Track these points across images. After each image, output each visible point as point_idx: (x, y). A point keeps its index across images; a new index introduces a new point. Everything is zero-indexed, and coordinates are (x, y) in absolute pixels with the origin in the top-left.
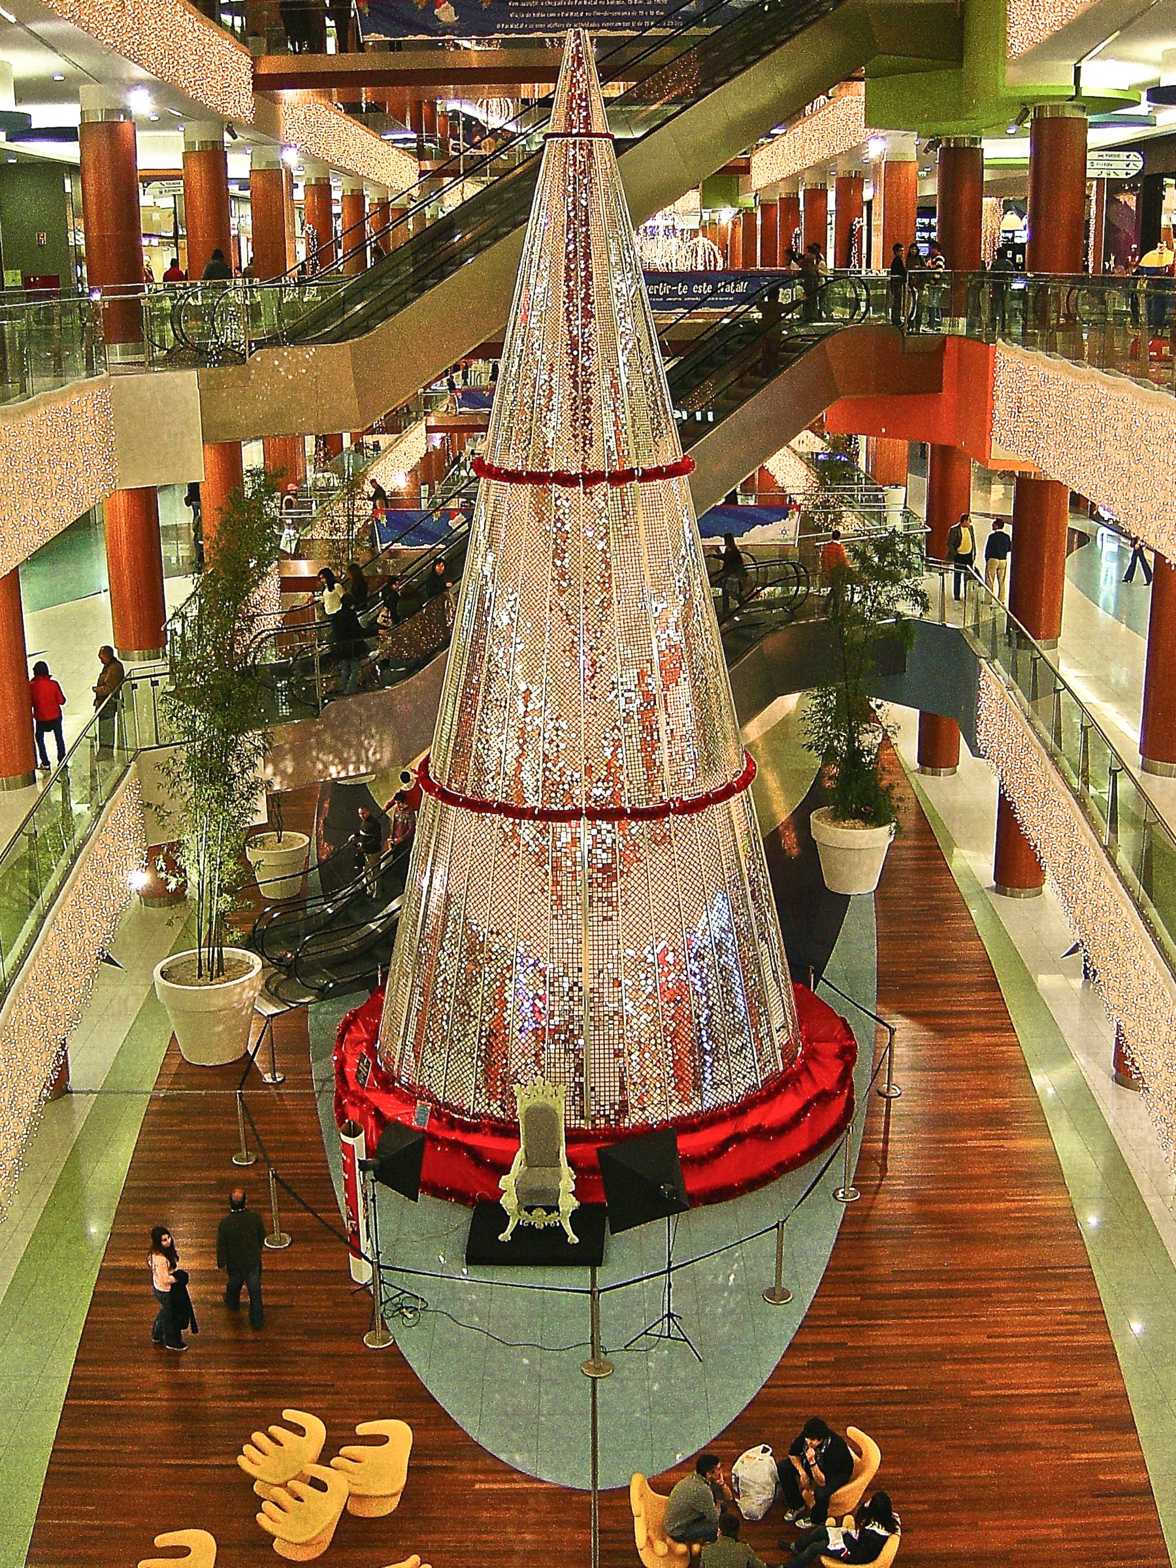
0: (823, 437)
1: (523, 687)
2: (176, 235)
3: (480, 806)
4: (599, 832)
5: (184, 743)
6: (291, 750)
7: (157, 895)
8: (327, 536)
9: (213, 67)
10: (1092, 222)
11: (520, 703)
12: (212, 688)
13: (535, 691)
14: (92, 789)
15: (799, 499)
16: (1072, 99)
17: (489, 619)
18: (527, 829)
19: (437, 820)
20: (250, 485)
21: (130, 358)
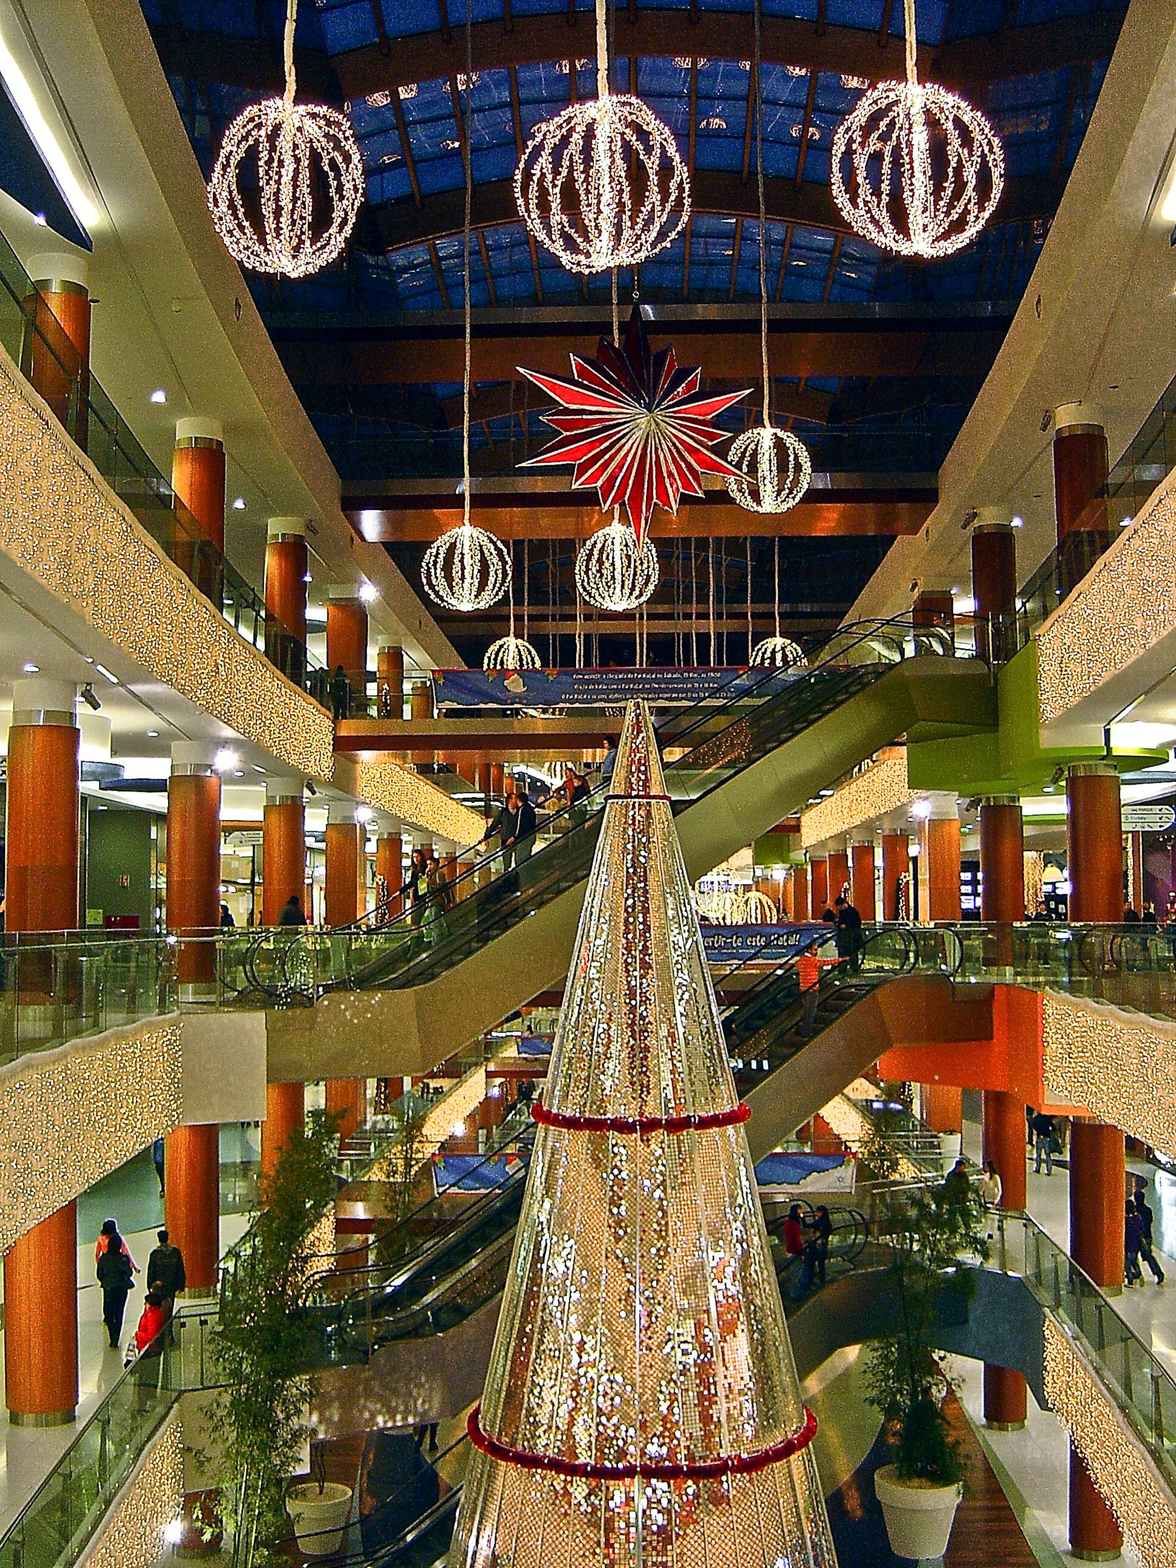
0: (877, 1086)
1: (577, 1337)
2: (253, 883)
3: (530, 1461)
4: (654, 1491)
5: (230, 1386)
6: (337, 1398)
7: (192, 1546)
8: (384, 1179)
9: (297, 729)
10: (1130, 872)
11: (574, 1354)
12: (261, 1329)
13: (590, 1341)
14: (132, 1430)
15: (855, 1147)
16: (1103, 758)
17: (544, 1267)
18: (579, 1488)
19: (485, 1476)
20: (311, 1125)
21: (204, 999)
